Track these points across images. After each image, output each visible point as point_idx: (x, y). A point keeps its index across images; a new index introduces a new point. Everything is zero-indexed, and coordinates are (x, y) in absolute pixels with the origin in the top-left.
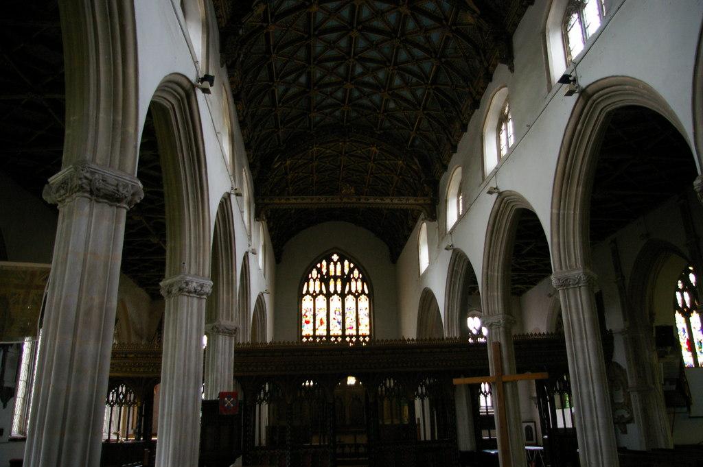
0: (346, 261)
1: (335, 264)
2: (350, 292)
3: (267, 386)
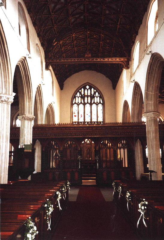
0: (93, 88)
1: (88, 90)
2: (94, 103)
3: (69, 142)
